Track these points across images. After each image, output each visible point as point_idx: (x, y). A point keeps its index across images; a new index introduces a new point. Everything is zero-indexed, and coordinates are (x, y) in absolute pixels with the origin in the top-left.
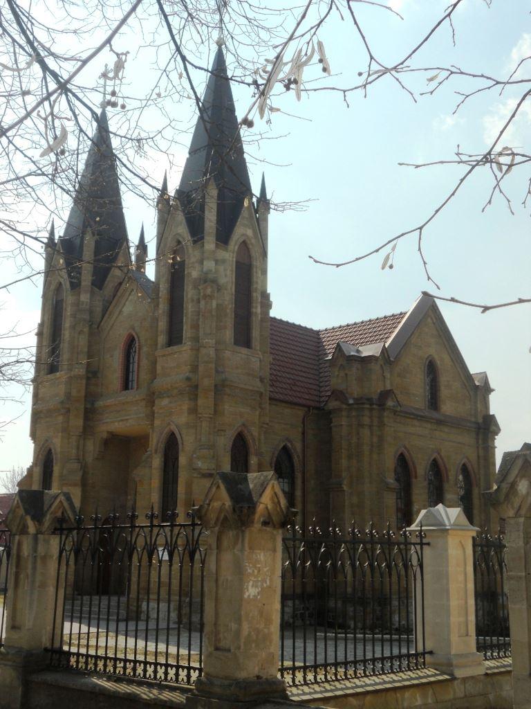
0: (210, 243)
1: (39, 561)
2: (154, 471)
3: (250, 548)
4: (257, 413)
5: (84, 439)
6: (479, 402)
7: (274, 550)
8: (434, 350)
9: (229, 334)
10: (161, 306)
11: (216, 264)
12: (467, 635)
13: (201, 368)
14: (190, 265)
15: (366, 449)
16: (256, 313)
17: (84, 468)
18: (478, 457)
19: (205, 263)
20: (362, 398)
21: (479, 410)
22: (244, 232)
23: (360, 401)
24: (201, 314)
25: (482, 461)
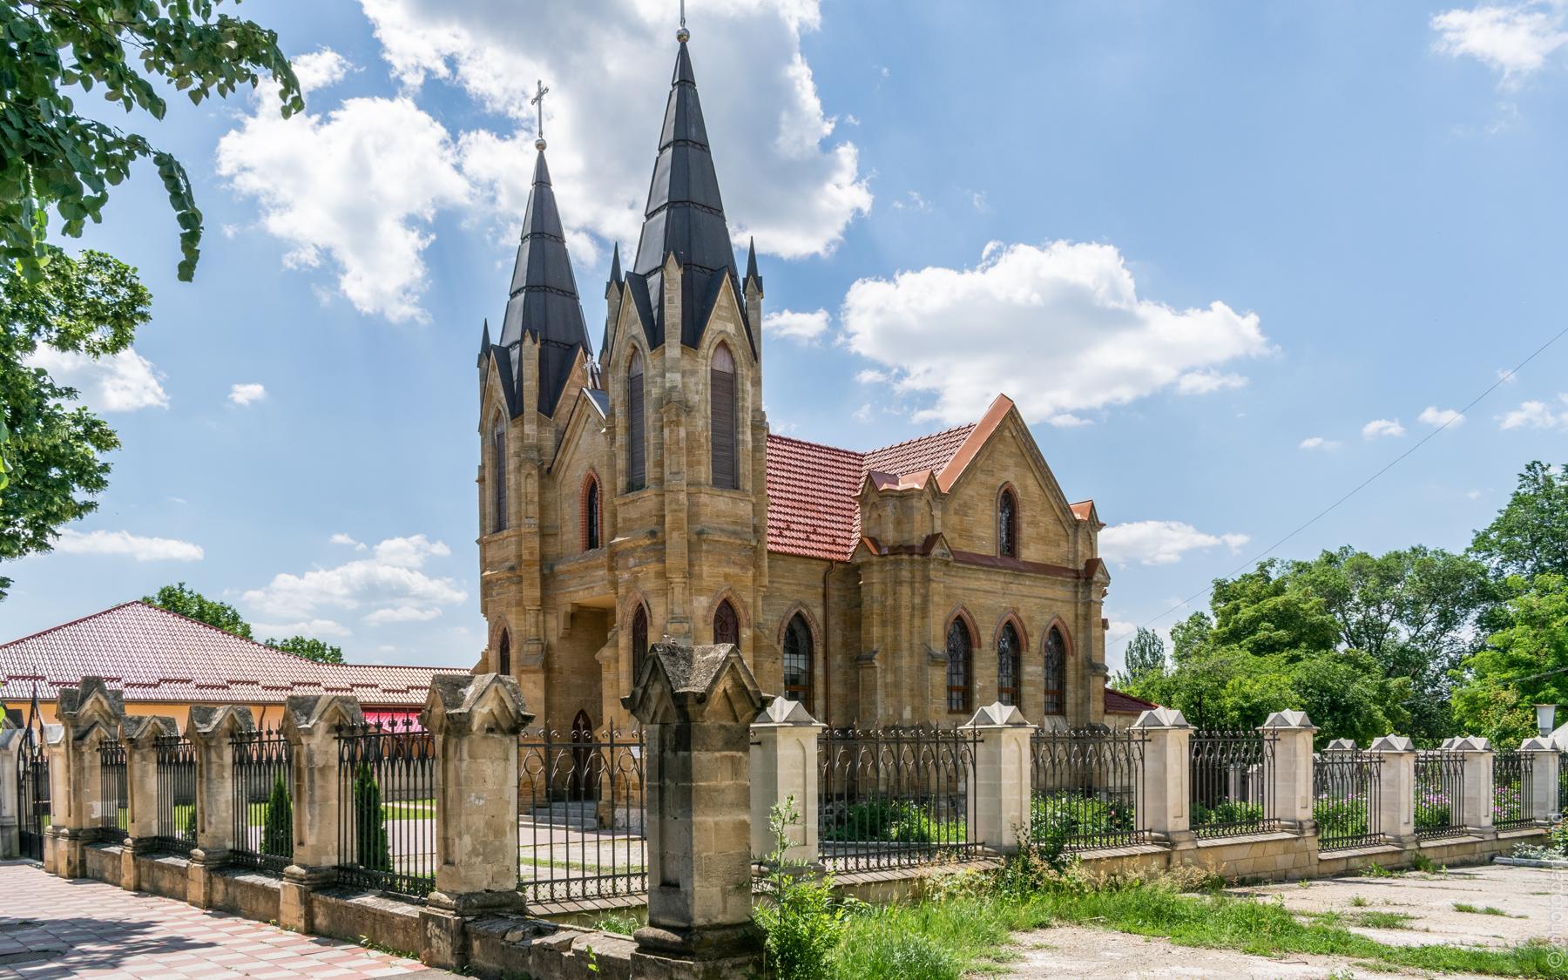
0: (673, 348)
1: (317, 776)
2: (621, 652)
3: (471, 757)
4: (750, 573)
5: (545, 614)
6: (1080, 542)
7: (507, 759)
8: (1013, 474)
9: (705, 472)
10: (618, 438)
11: (683, 377)
12: (805, 844)
13: (668, 519)
14: (650, 380)
15: (905, 613)
16: (743, 440)
17: (547, 651)
18: (1077, 616)
19: (667, 375)
20: (901, 546)
21: (1080, 554)
22: (723, 329)
23: (897, 550)
24: (665, 446)
25: (1081, 622)
